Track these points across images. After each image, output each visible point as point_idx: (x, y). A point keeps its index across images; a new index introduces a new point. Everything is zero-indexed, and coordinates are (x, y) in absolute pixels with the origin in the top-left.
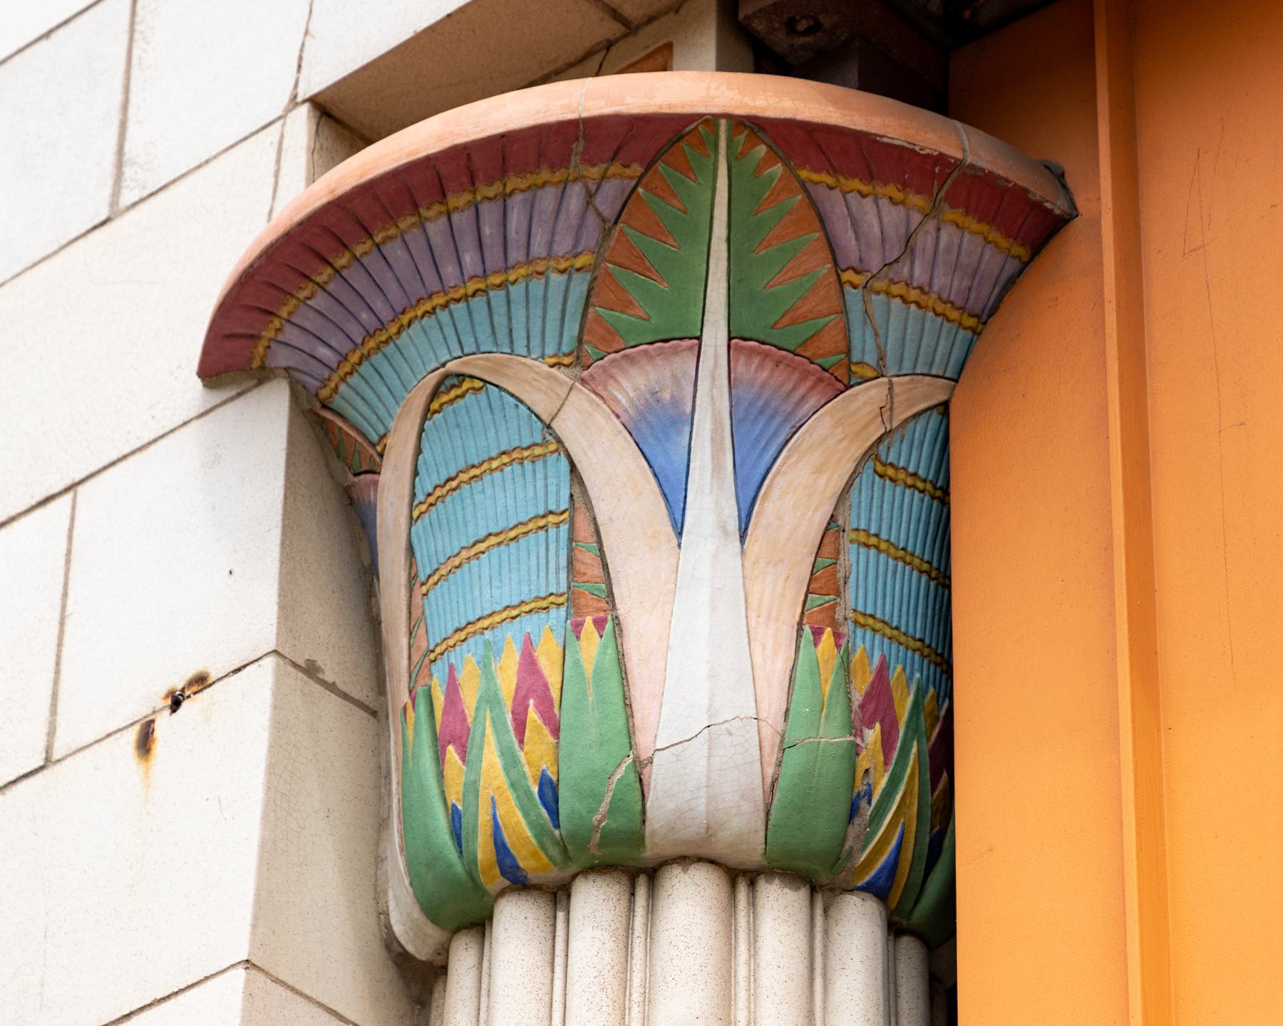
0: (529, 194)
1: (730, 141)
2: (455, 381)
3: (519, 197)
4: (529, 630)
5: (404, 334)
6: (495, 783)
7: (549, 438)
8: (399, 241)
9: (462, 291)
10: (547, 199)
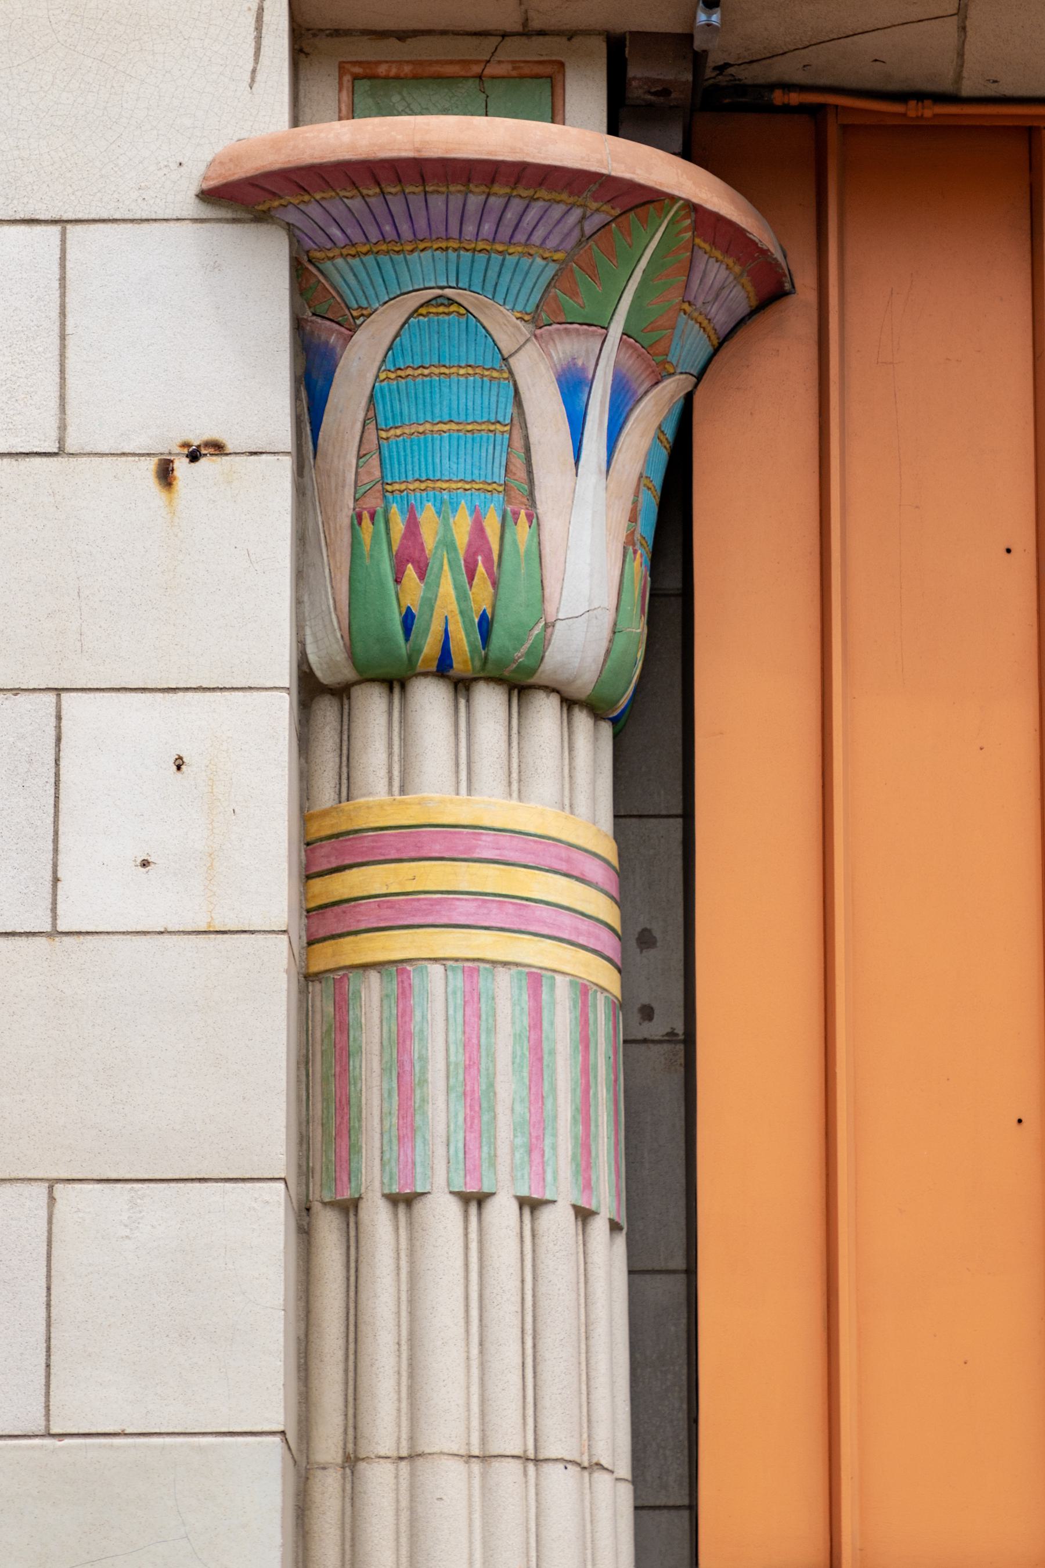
0: (547, 204)
1: (676, 212)
2: (446, 302)
3: (540, 203)
4: (477, 503)
5: (416, 254)
6: (450, 607)
7: (504, 368)
8: (444, 196)
9: (473, 246)
10: (557, 211)
